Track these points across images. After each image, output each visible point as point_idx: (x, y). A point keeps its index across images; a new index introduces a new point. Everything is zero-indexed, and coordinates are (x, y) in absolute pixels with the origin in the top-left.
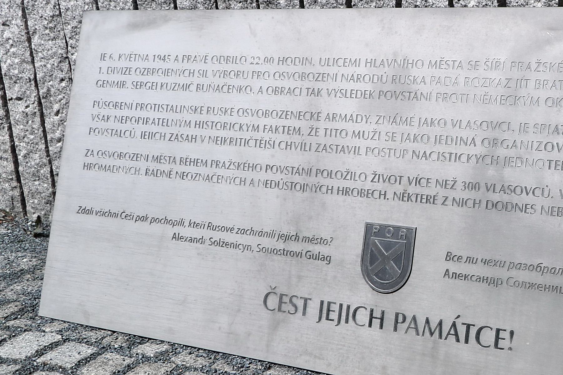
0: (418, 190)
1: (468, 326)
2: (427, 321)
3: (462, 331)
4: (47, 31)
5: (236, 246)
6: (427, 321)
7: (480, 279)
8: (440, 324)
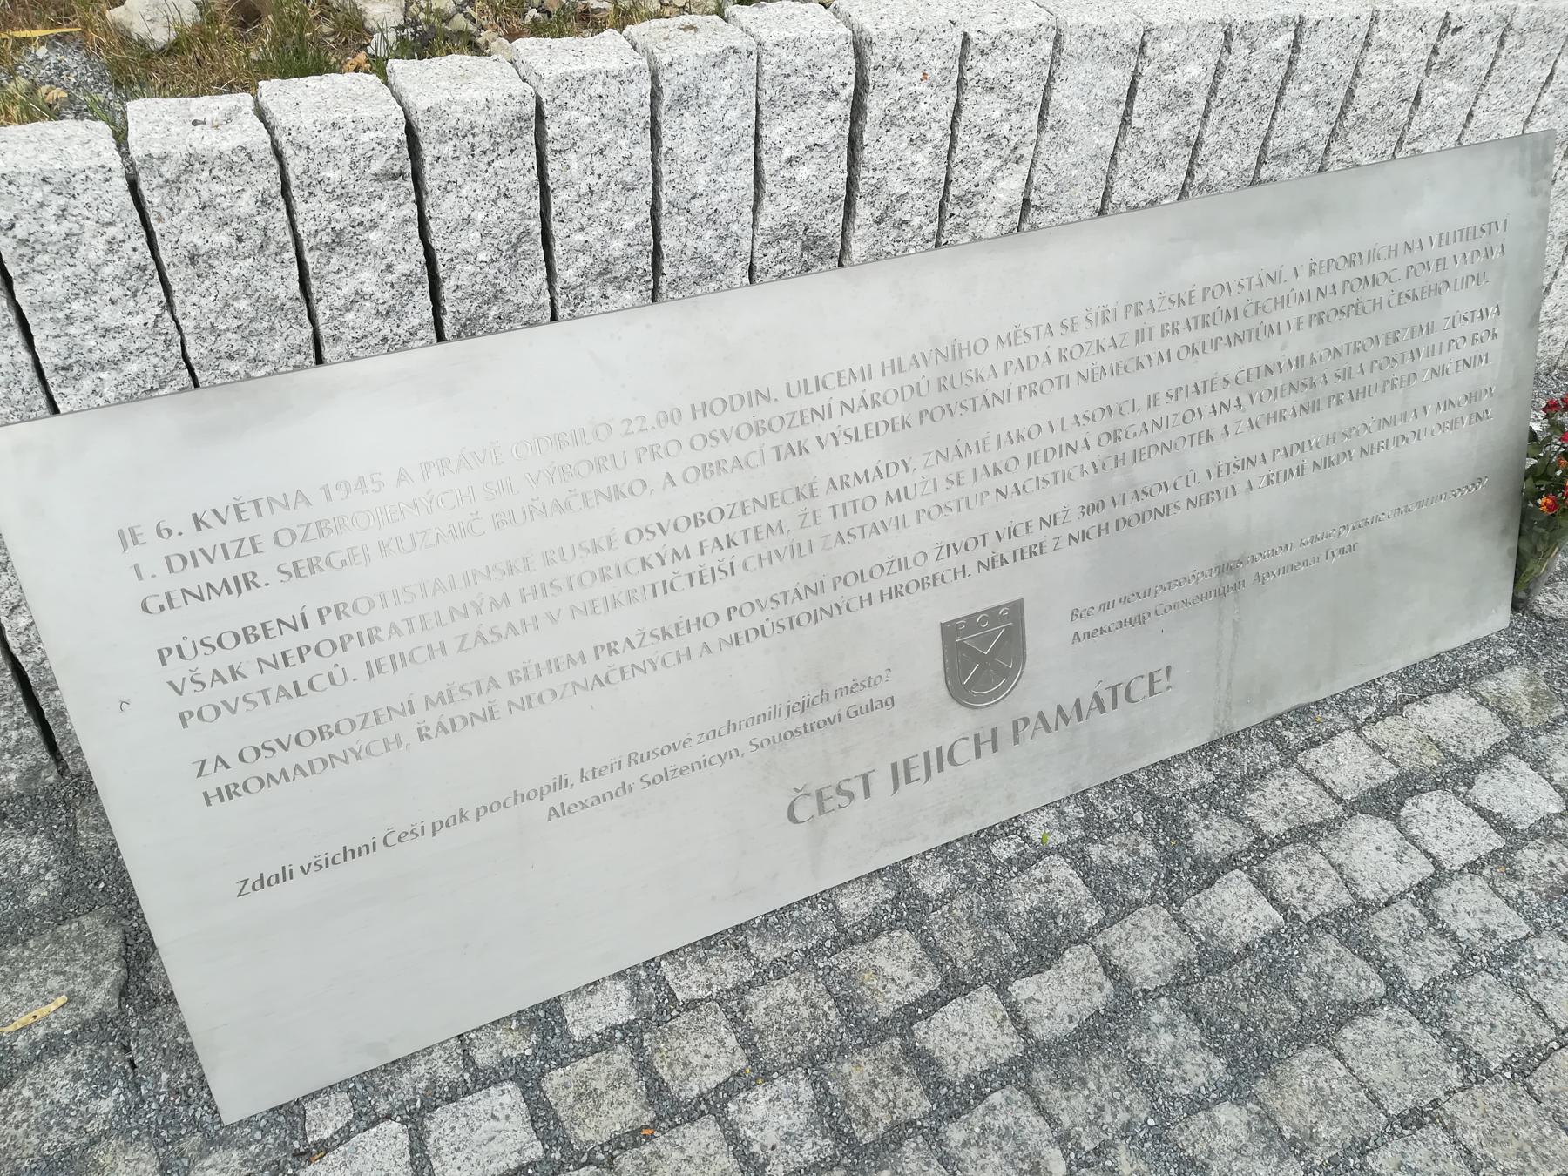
0: (1015, 543)
2: (1060, 709)
3: (1106, 696)
6: (1060, 709)
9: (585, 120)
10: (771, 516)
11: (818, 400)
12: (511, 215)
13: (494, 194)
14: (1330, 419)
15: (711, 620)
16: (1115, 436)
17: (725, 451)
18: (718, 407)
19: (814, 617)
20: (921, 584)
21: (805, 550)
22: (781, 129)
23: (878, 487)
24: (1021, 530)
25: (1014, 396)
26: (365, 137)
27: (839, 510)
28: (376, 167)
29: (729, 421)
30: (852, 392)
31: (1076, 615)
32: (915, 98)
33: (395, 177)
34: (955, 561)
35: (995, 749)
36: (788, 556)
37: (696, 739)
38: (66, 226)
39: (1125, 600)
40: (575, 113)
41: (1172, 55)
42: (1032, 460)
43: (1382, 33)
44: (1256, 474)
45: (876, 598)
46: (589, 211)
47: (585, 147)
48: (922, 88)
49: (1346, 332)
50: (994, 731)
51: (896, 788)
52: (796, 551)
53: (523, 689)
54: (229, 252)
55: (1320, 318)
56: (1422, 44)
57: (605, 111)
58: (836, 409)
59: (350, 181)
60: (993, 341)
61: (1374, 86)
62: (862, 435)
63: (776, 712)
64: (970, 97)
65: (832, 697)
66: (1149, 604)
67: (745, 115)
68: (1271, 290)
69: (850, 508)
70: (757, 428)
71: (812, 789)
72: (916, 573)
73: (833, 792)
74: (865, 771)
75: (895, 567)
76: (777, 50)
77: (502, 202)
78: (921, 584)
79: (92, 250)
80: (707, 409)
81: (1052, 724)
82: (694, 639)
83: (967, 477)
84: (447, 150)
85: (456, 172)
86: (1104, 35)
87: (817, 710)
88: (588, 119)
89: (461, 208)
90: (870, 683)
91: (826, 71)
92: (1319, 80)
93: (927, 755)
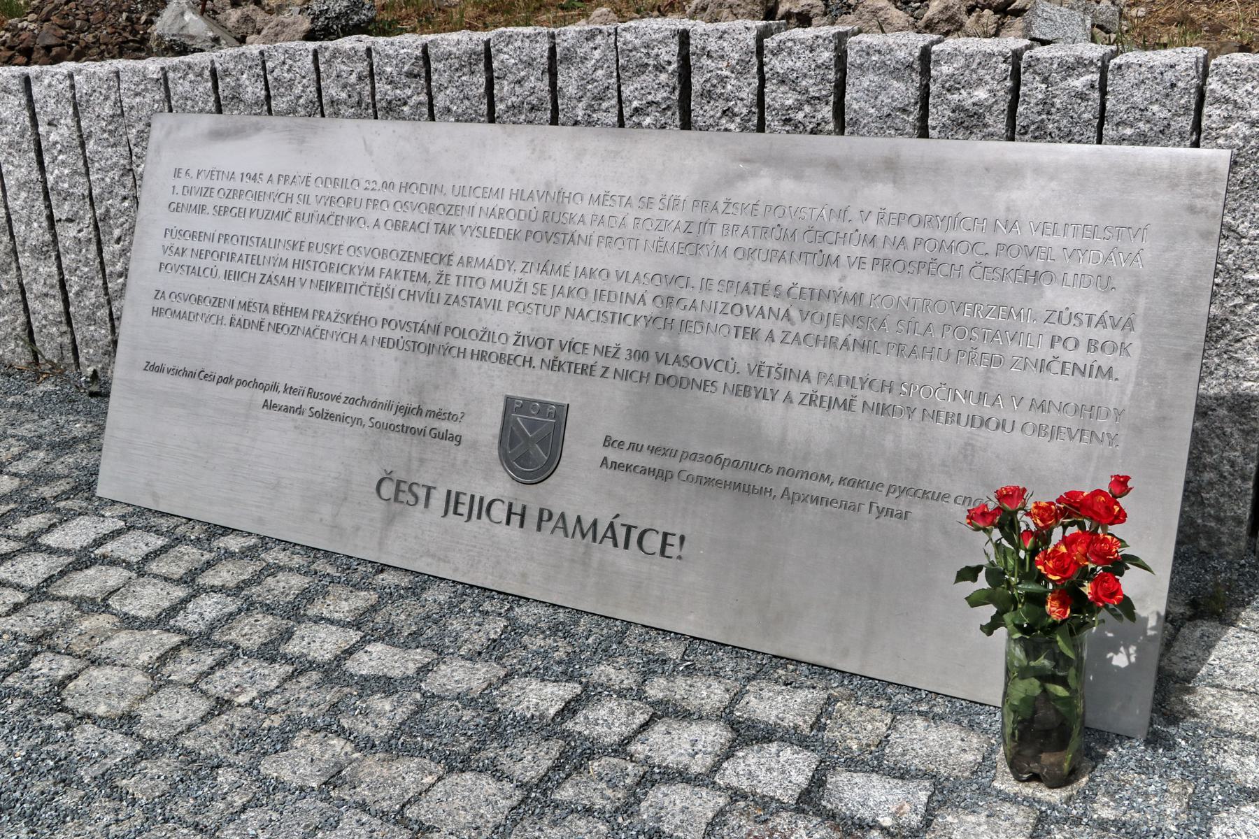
0: (572, 357)
1: (629, 528)
2: (579, 520)
3: (621, 533)
4: (106, 135)
5: (343, 419)
6: (579, 520)
7: (645, 471)
8: (595, 524)
12: (470, 111)
14: (887, 366)
16: (669, 301)
19: (429, 349)
20: (500, 358)
21: (435, 300)
22: (632, 88)
23: (489, 274)
24: (579, 348)
25: (594, 243)
26: (402, 51)
27: (462, 280)
29: (416, 198)
30: (491, 203)
31: (608, 442)
32: (723, 80)
33: (415, 76)
34: (524, 351)
35: (522, 525)
39: (653, 450)
42: (599, 295)
44: (797, 389)
47: (511, 77)
48: (726, 73)
49: (910, 288)
50: (524, 508)
52: (429, 297)
55: (882, 263)
59: (395, 74)
60: (587, 197)
63: (387, 406)
64: (769, 87)
66: (673, 465)
67: (609, 76)
74: (430, 484)
76: (624, 33)
77: (467, 103)
78: (500, 358)
79: (298, 90)
81: (570, 531)
84: (440, 66)
85: (444, 81)
86: (879, 52)
87: (420, 421)
90: (451, 417)
91: (656, 50)
92: (1141, 124)
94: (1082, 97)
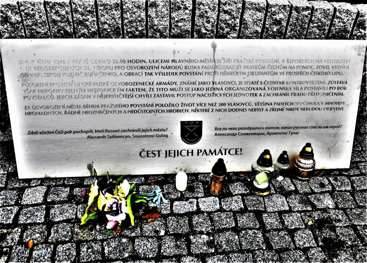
0: (201, 107)
7: (228, 135)
9: (130, 6)
10: (143, 87)
11: (156, 65)
12: (115, 23)
13: (111, 18)
15: (127, 106)
17: (134, 71)
18: (134, 61)
21: (150, 96)
22: (175, 14)
23: (169, 87)
24: (203, 105)
27: (159, 89)
28: (88, 9)
30: (164, 64)
31: (216, 129)
32: (206, 12)
36: (146, 96)
37: (120, 131)
38: (33, 12)
40: (129, 5)
41: (275, 11)
43: (338, 14)
45: (165, 111)
46: (131, 25)
51: (166, 156)
52: (147, 96)
53: (86, 109)
54: (61, 21)
56: (350, 19)
57: (135, 5)
58: (160, 68)
61: (337, 27)
62: (166, 74)
65: (153, 131)
68: (275, 64)
69: (161, 90)
70: (142, 68)
71: (146, 150)
72: (176, 108)
73: (150, 152)
75: (171, 105)
77: (113, 20)
80: (131, 61)
82: (123, 109)
83: (191, 89)
88: (132, 6)
89: (105, 20)
90: (164, 130)
92: (319, 23)
93: (175, 151)
94: (307, 16)
